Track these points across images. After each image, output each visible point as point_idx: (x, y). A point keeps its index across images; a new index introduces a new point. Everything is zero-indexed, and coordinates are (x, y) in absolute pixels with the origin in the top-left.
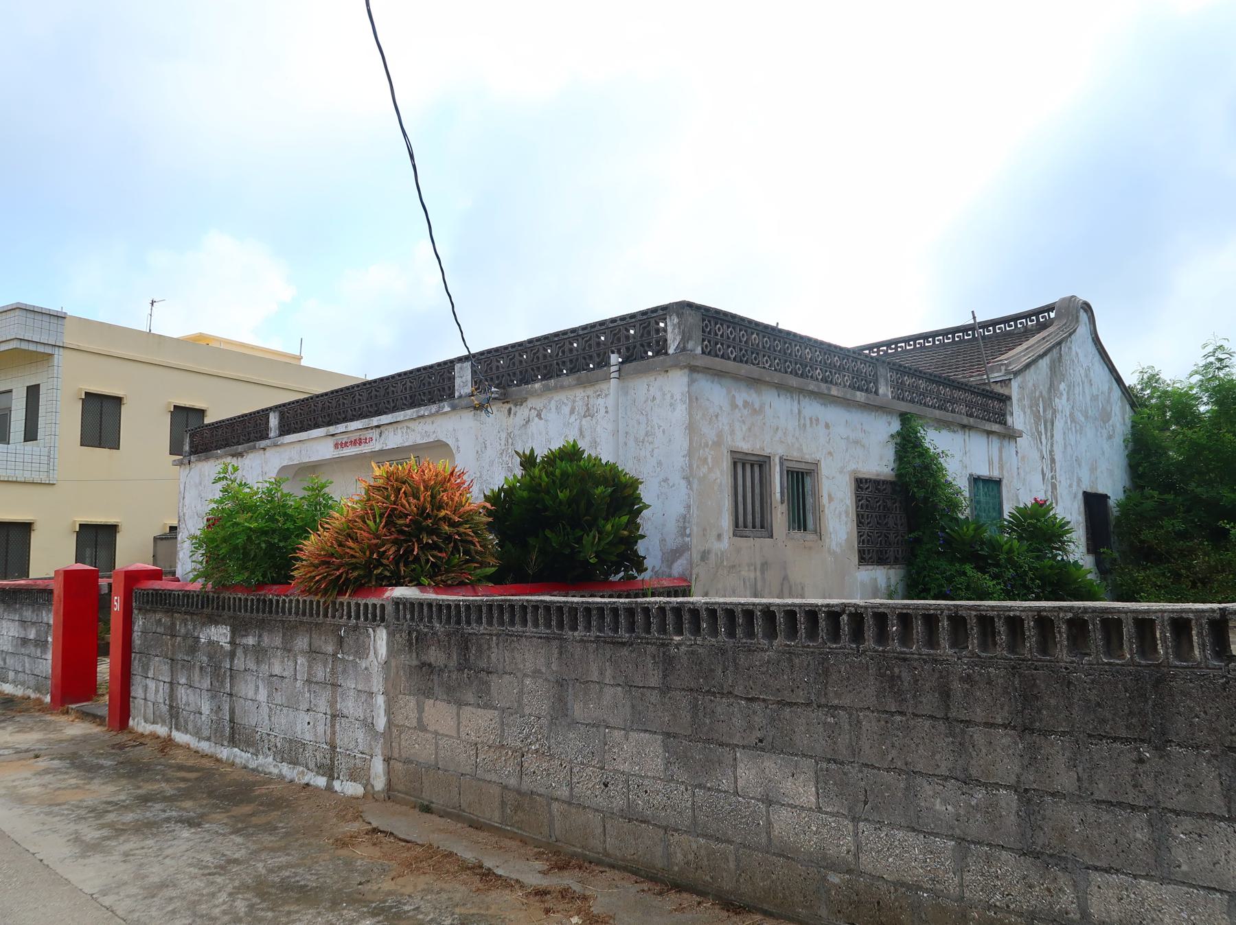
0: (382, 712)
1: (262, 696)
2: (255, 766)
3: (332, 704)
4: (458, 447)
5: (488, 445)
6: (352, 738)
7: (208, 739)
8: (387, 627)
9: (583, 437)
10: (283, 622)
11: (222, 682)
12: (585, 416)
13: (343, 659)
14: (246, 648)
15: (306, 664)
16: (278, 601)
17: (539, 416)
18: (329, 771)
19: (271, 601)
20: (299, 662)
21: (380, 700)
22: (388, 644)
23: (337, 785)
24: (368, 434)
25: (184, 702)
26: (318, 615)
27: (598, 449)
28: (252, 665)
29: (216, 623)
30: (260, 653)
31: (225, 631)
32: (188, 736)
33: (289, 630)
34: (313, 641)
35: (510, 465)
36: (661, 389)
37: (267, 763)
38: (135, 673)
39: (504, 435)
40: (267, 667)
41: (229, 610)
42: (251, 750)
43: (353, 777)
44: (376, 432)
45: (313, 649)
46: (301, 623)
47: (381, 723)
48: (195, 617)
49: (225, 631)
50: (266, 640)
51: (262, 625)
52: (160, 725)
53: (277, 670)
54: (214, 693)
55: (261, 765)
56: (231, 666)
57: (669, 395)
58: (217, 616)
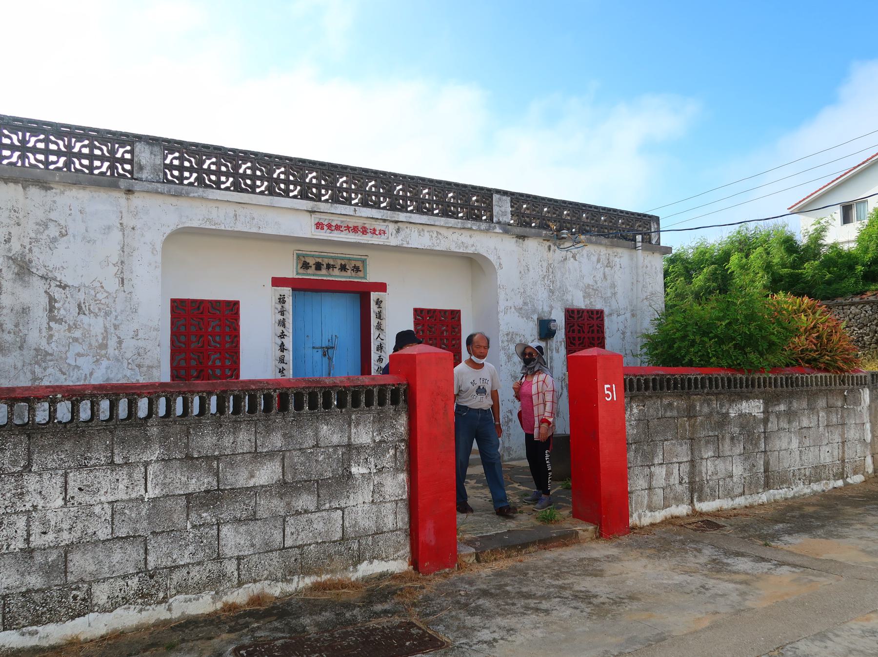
0: (869, 432)
1: (795, 444)
2: (792, 495)
3: (842, 435)
4: (500, 264)
5: (531, 269)
6: (854, 452)
7: (743, 494)
8: (869, 388)
9: (606, 280)
10: (807, 391)
11: (756, 444)
12: (607, 267)
13: (848, 408)
14: (778, 415)
15: (825, 415)
16: (802, 378)
17: (574, 257)
18: (841, 475)
19: (797, 378)
20: (820, 415)
21: (868, 426)
22: (870, 395)
23: (849, 480)
24: (379, 226)
25: (710, 473)
26: (831, 384)
27: (616, 289)
28: (784, 424)
29: (748, 398)
30: (791, 415)
31: (758, 404)
32: (717, 500)
33: (812, 396)
34: (828, 401)
35: (551, 288)
36: (650, 262)
37: (802, 489)
38: (629, 465)
39: (545, 264)
40: (797, 423)
41: (759, 387)
42: (785, 486)
43: (855, 473)
44: (392, 227)
45: (829, 406)
46: (821, 391)
47: (869, 437)
48: (722, 396)
49: (758, 404)
50: (795, 405)
51: (791, 395)
52: (674, 506)
53: (805, 423)
54: (746, 456)
55: (796, 492)
56: (765, 429)
57: (654, 267)
58: (748, 392)
